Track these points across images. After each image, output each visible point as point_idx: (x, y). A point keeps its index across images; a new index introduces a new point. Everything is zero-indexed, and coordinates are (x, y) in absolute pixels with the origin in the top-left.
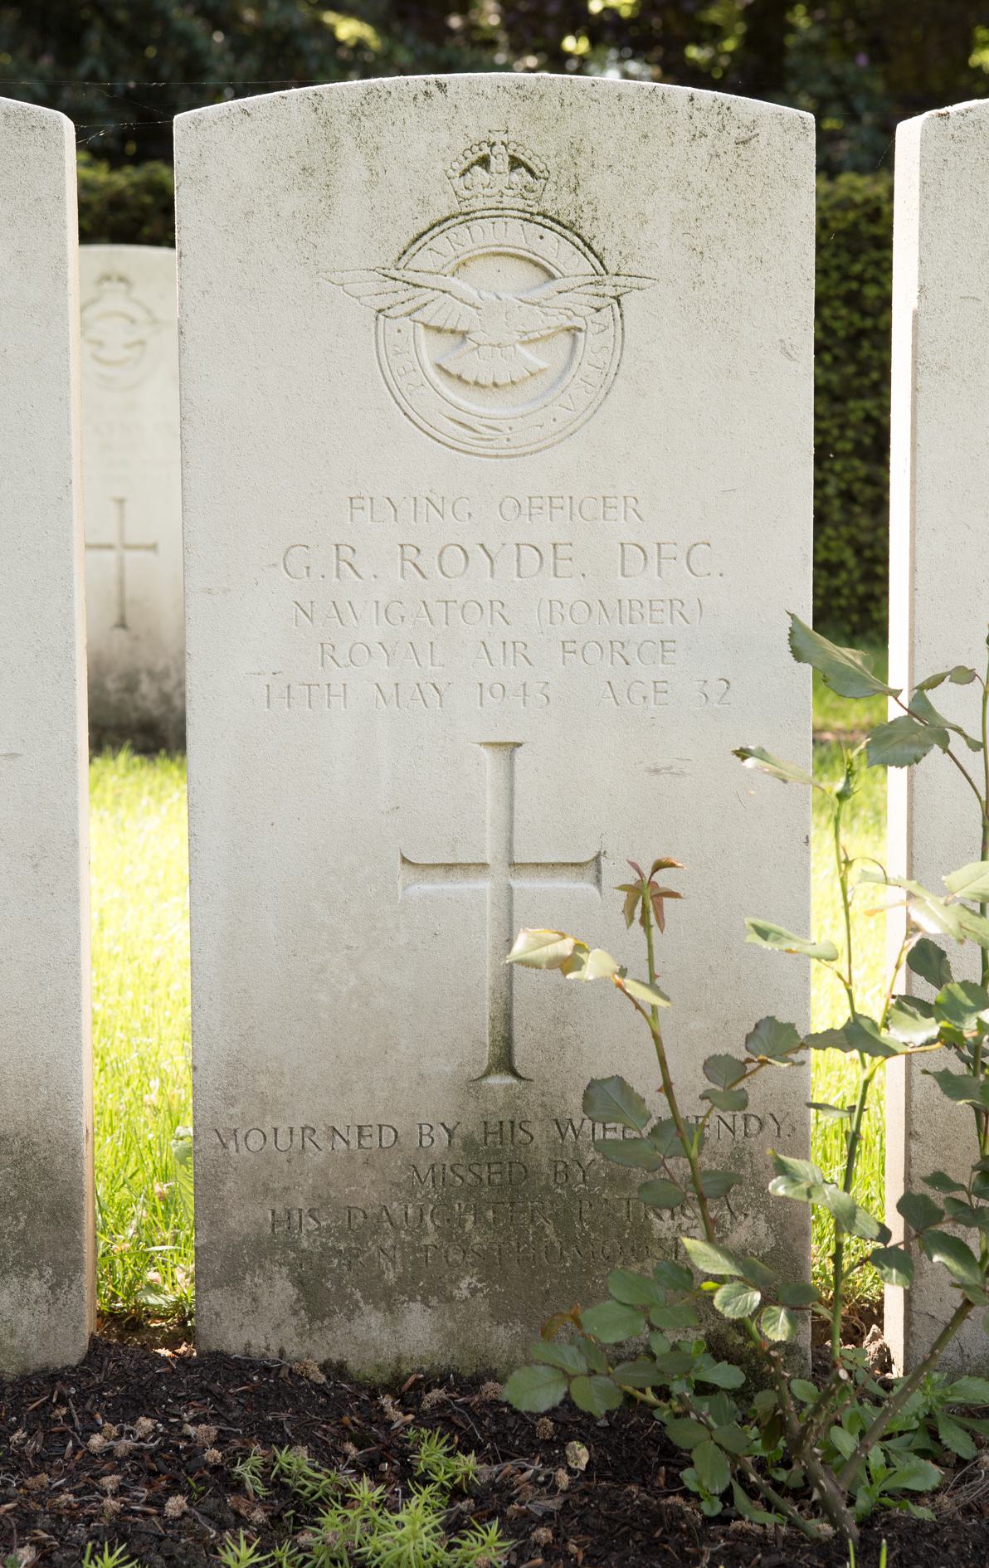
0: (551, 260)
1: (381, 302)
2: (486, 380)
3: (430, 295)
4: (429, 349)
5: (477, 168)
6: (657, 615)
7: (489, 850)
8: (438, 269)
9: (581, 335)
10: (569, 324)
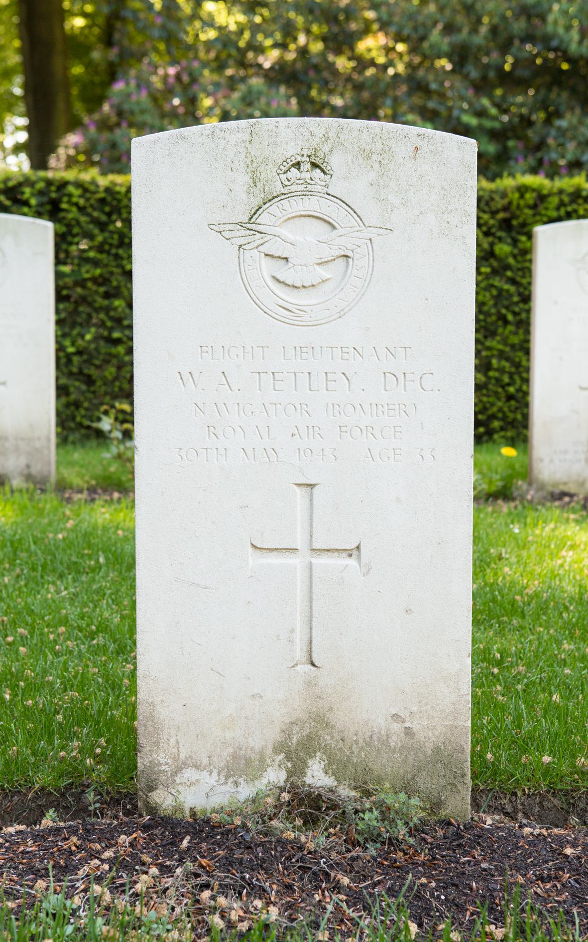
0: (335, 219)
1: (242, 241)
2: (298, 284)
3: (269, 237)
4: (267, 267)
5: (293, 169)
6: (392, 412)
7: (300, 542)
8: (247, 221)
9: (350, 260)
10: (344, 253)
